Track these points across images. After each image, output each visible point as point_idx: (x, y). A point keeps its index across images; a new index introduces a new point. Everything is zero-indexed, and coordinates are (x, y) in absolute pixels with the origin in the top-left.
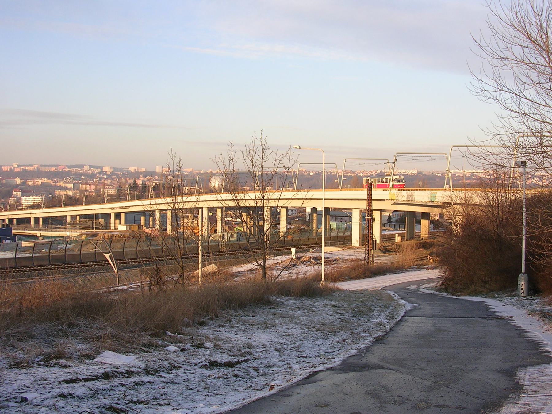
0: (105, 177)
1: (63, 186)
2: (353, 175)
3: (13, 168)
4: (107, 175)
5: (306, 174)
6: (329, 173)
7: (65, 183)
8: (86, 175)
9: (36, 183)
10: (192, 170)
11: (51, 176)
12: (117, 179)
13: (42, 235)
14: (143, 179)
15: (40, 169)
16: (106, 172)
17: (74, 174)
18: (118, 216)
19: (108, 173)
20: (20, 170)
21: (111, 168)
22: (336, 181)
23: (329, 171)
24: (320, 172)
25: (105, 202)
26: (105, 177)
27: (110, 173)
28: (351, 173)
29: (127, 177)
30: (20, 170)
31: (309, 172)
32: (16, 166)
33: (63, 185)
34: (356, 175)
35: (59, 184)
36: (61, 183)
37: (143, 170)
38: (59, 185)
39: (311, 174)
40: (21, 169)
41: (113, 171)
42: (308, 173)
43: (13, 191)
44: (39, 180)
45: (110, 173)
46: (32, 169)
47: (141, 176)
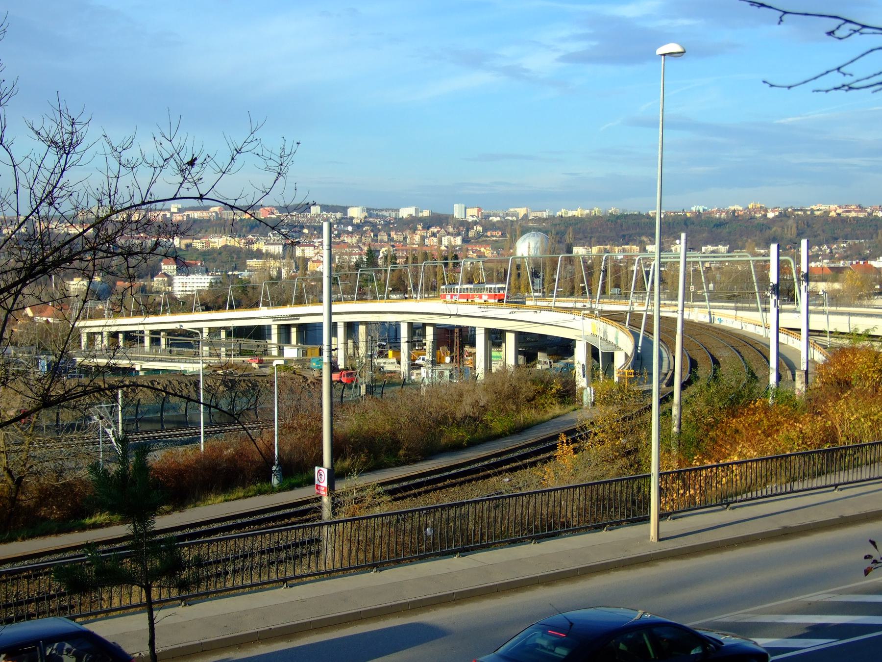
0: (350, 228)
1: (264, 251)
2: (861, 215)
3: (168, 215)
4: (352, 225)
5: (758, 215)
6: (809, 213)
7: (267, 243)
8: (312, 227)
9: (211, 245)
10: (525, 212)
11: (244, 229)
12: (372, 235)
13: (143, 367)
14: (423, 233)
15: (224, 216)
16: (352, 218)
17: (288, 225)
18: (285, 330)
19: (355, 221)
20: (183, 218)
21: (363, 211)
22: (581, 285)
23: (789, 206)
24: (790, 210)
25: (106, 315)
26: (350, 228)
27: (359, 221)
28: (856, 211)
29: (391, 229)
30: (183, 218)
31: (766, 210)
32: (176, 210)
33: (264, 248)
34: (866, 214)
35: (255, 247)
36: (260, 245)
37: (426, 213)
38: (255, 249)
39: (771, 215)
40: (185, 217)
41: (366, 217)
42: (763, 213)
43: (162, 264)
44: (216, 240)
45: (359, 221)
46: (207, 216)
47: (419, 227)
